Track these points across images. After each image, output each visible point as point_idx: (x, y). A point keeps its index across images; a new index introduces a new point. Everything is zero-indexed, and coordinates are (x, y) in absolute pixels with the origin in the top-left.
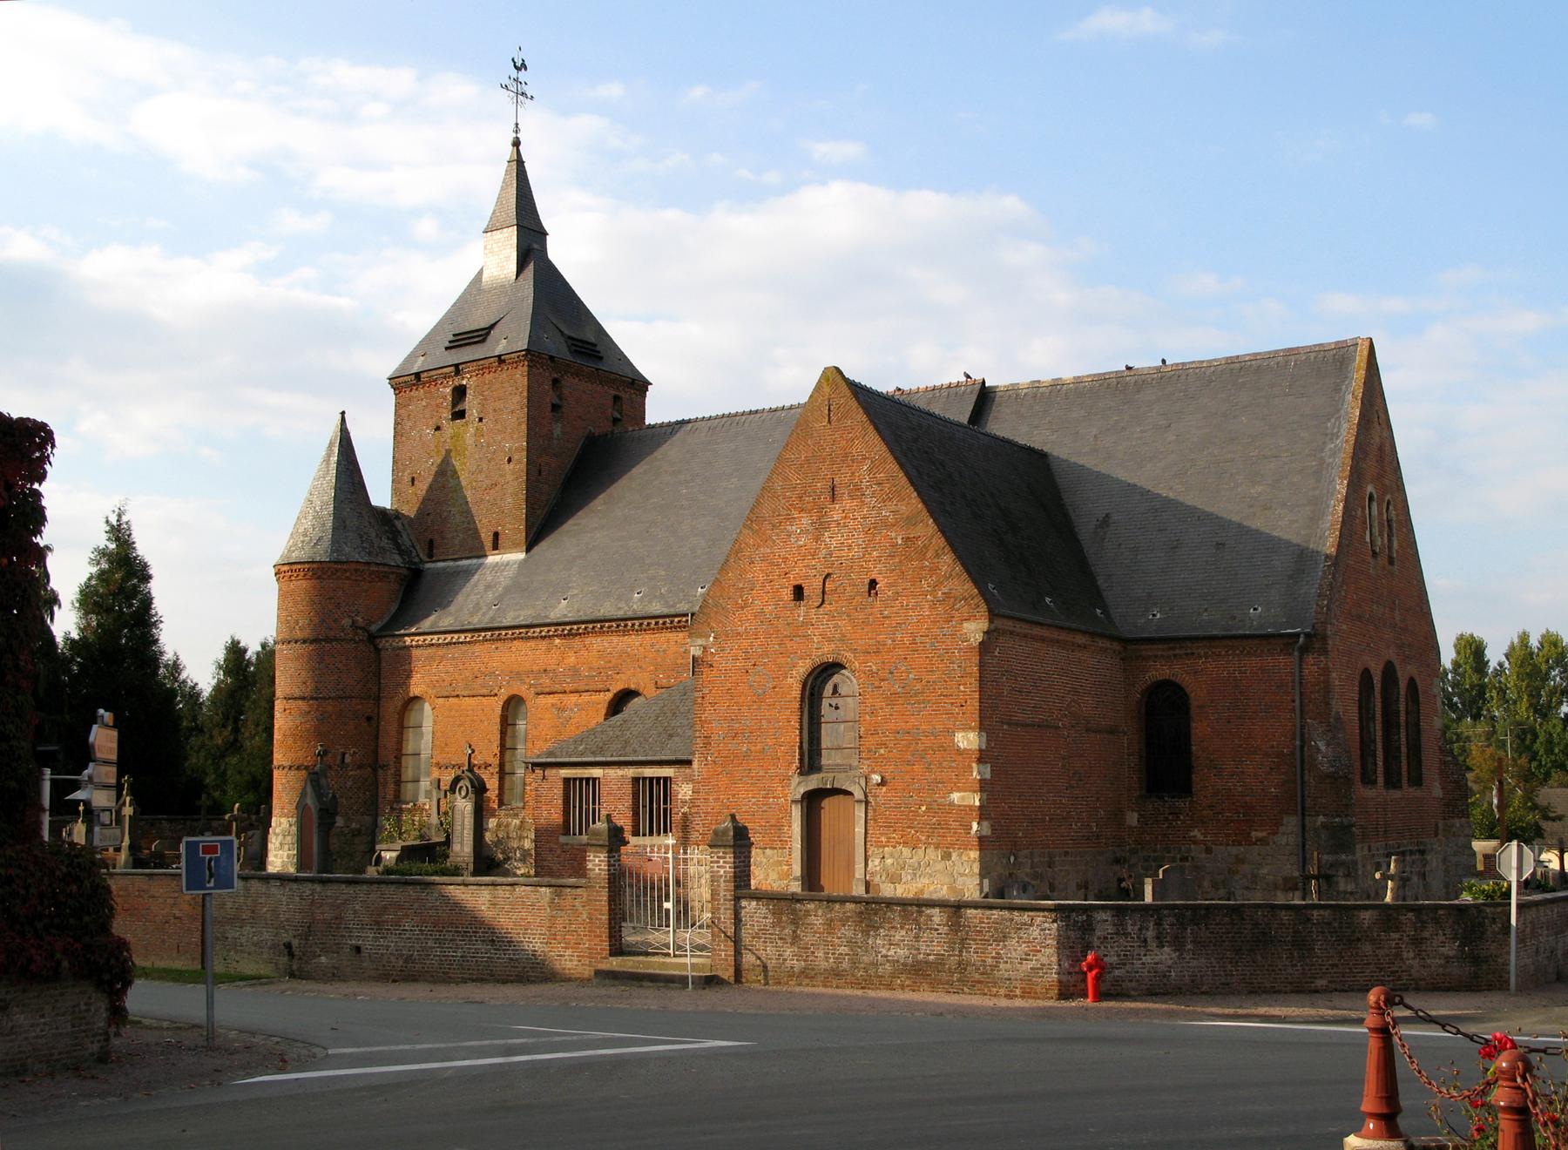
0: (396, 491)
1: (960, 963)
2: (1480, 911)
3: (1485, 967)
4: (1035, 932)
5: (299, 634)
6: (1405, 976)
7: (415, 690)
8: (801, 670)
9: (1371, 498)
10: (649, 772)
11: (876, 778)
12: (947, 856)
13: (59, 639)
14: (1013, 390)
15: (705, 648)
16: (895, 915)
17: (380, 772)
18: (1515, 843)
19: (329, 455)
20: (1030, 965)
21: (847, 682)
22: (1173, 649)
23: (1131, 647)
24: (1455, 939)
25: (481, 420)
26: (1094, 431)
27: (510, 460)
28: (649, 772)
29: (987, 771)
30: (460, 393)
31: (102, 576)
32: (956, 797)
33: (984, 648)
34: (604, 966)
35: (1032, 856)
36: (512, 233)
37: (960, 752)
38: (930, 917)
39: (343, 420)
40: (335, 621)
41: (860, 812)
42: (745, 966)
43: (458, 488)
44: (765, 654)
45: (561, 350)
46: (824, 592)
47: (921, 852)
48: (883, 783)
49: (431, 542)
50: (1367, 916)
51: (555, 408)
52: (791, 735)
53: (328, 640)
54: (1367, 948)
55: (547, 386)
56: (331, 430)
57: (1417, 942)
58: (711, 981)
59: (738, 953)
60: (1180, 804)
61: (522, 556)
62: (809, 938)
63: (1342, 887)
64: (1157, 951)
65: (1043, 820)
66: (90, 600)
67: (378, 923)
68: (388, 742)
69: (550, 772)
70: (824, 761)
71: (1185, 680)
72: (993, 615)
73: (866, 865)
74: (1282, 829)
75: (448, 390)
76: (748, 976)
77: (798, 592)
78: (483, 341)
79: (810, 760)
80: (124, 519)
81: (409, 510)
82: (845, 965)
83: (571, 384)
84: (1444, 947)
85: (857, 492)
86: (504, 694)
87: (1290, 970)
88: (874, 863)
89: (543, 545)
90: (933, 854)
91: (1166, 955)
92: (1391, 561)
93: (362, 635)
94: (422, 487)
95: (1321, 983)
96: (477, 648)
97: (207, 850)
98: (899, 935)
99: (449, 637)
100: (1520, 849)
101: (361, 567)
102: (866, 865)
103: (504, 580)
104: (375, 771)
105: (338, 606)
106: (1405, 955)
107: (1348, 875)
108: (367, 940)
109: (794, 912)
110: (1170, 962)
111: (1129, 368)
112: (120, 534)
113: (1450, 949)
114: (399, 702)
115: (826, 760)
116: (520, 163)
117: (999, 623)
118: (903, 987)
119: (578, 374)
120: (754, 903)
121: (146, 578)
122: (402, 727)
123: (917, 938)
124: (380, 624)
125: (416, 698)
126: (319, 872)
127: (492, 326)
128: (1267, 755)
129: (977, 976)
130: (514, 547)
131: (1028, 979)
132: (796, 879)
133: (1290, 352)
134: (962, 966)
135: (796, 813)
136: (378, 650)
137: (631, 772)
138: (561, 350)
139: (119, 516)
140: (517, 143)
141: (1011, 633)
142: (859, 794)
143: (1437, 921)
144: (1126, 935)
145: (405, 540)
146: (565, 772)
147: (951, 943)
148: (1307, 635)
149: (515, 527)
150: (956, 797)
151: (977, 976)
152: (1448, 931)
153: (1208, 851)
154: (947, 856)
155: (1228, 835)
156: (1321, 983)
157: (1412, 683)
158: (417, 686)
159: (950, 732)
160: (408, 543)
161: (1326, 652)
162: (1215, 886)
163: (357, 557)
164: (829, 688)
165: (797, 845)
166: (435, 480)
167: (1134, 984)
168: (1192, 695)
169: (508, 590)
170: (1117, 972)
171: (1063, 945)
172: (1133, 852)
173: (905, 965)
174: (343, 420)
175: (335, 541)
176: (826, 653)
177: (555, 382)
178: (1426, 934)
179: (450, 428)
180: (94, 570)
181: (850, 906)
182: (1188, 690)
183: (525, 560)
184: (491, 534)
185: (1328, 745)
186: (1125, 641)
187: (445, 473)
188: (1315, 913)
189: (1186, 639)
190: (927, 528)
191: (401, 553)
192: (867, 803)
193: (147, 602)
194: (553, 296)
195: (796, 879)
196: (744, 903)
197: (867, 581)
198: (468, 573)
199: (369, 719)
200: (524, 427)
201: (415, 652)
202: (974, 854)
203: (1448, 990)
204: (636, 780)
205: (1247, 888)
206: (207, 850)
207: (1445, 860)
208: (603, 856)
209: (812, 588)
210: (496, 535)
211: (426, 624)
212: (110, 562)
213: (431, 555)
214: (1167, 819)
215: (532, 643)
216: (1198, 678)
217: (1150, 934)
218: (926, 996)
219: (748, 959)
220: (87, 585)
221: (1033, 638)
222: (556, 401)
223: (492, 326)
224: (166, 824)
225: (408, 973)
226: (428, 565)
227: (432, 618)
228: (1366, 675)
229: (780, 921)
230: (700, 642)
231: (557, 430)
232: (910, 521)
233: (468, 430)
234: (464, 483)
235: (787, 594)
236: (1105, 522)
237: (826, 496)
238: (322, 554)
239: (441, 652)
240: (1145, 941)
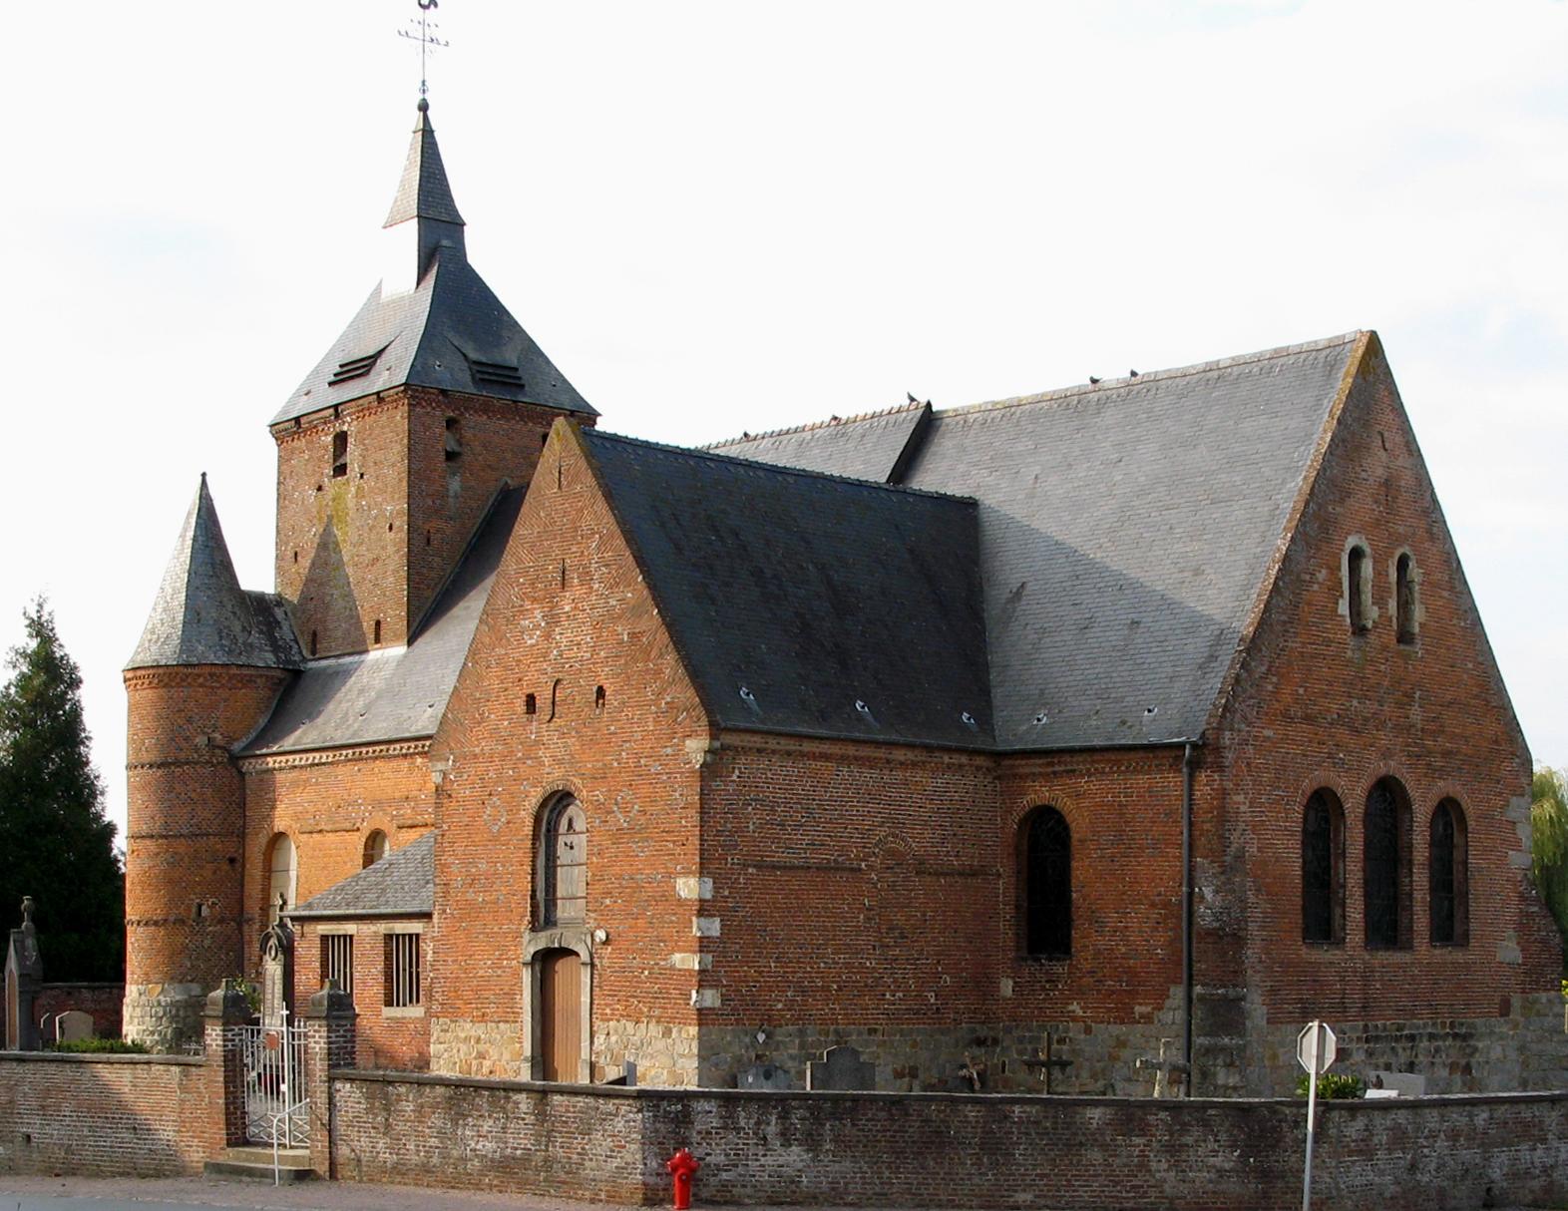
1: (545, 1161)
2: (1275, 1112)
3: (1280, 1184)
4: (620, 1124)
5: (146, 758)
6: (1153, 1193)
7: (280, 825)
8: (534, 801)
9: (1356, 555)
10: (400, 927)
11: (601, 935)
12: (667, 1033)
14: (962, 415)
16: (483, 1100)
17: (246, 928)
18: (1315, 1024)
19: (185, 530)
21: (577, 814)
22: (1052, 764)
23: (1005, 763)
24: (1233, 1147)
25: (362, 476)
27: (391, 528)
28: (400, 927)
29: (714, 927)
30: (341, 440)
32: (677, 959)
33: (710, 771)
34: (221, 1159)
35: (802, 1033)
38: (517, 1103)
39: (204, 483)
40: (186, 739)
42: (341, 1160)
43: (340, 564)
46: (553, 703)
47: (643, 1026)
48: (607, 942)
49: (315, 634)
50: (1096, 1115)
51: (450, 456)
52: (520, 884)
53: (177, 763)
54: (1095, 1156)
55: (439, 429)
57: (1173, 1150)
58: (302, 1176)
59: (332, 1143)
60: (1060, 969)
61: (400, 650)
62: (401, 1127)
64: (781, 1150)
65: (826, 989)
67: (43, 1107)
68: (253, 889)
70: (559, 913)
71: (1065, 804)
73: (592, 1043)
74: (1168, 1003)
75: (330, 438)
77: (531, 701)
78: (367, 373)
79: (543, 914)
81: (292, 595)
83: (475, 424)
86: (366, 829)
87: (976, 1180)
88: (600, 1039)
90: (655, 1030)
91: (794, 1157)
94: (305, 562)
98: (486, 1125)
99: (311, 756)
100: (1321, 1027)
101: (218, 671)
102: (592, 1043)
103: (378, 683)
104: (240, 925)
106: (1154, 1165)
107: (1229, 1065)
108: (34, 1126)
109: (386, 1096)
110: (800, 1165)
111: (1094, 381)
112: (41, 630)
113: (1226, 1160)
114: (264, 839)
116: (427, 134)
117: (729, 739)
118: (491, 1187)
119: (486, 409)
120: (348, 1086)
121: (75, 683)
122: (269, 870)
123: (504, 1128)
126: (21, 1050)
127: (380, 352)
128: (1153, 905)
129: (563, 1176)
130: (396, 638)
131: (612, 1181)
132: (526, 1059)
133: (1278, 354)
135: (526, 975)
136: (242, 775)
137: (382, 927)
139: (40, 606)
141: (759, 751)
142: (584, 956)
143: (1206, 1124)
144: (738, 1130)
145: (285, 633)
147: (538, 1135)
148: (1194, 746)
149: (396, 616)
151: (563, 1176)
152: (1223, 1137)
153: (1088, 1030)
154: (667, 1033)
155: (1110, 1010)
157: (1448, 812)
159: (670, 876)
160: (289, 637)
162: (1094, 1077)
163: (212, 659)
164: (564, 823)
166: (317, 555)
167: (749, 1191)
168: (1073, 826)
170: (724, 1176)
171: (651, 1141)
173: (492, 1160)
174: (204, 483)
175: (186, 639)
176: (554, 777)
177: (451, 424)
178: (1189, 1140)
179: (332, 486)
181: (440, 1090)
182: (1069, 819)
183: (405, 656)
184: (373, 623)
185: (1216, 892)
186: (999, 756)
187: (327, 545)
188: (1017, 1109)
189: (1061, 751)
190: (651, 619)
191: (276, 648)
192: (593, 965)
193: (76, 714)
195: (526, 1059)
196: (338, 1085)
197: (595, 689)
198: (345, 674)
199: (232, 861)
200: (405, 484)
201: (280, 777)
202: (693, 1030)
204: (388, 937)
205: (1129, 1080)
207: (1522, 1049)
208: (219, 1029)
210: (378, 623)
211: (288, 743)
212: (31, 663)
213: (314, 653)
214: (1043, 988)
215: (394, 764)
216: (1080, 801)
219: (343, 1151)
222: (452, 446)
223: (380, 352)
224: (86, 994)
225: (66, 1168)
226: (312, 665)
227: (298, 733)
229: (373, 1106)
230: (440, 766)
231: (455, 485)
232: (636, 612)
234: (345, 559)
235: (520, 706)
236: (1018, 595)
237: (556, 585)
238: (169, 654)
239: (306, 774)
240: (765, 1138)
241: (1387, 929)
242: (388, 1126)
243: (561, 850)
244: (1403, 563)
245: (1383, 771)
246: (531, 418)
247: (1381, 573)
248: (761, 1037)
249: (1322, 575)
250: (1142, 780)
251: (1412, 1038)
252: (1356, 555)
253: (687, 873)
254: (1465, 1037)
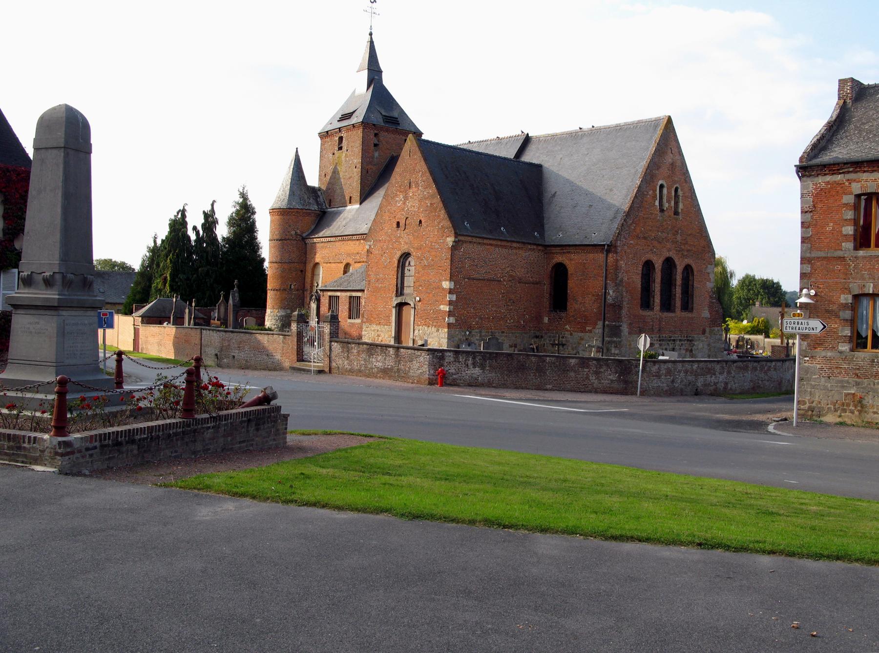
0: (320, 180)
4: (422, 359)
5: (275, 237)
6: (590, 387)
7: (317, 260)
9: (662, 186)
10: (354, 294)
11: (418, 299)
12: (438, 331)
13: (220, 239)
16: (379, 350)
23: (548, 249)
24: (616, 373)
26: (561, 156)
28: (354, 294)
29: (454, 298)
30: (341, 139)
33: (454, 248)
35: (480, 332)
36: (365, 73)
41: (412, 311)
43: (339, 178)
44: (387, 249)
45: (380, 121)
48: (420, 301)
51: (375, 145)
53: (285, 240)
54: (572, 374)
56: (292, 156)
57: (597, 373)
58: (320, 372)
60: (563, 314)
65: (489, 318)
66: (232, 222)
68: (308, 280)
69: (325, 293)
71: (566, 262)
72: (456, 235)
76: (334, 371)
77: (398, 224)
81: (324, 188)
83: (383, 135)
84: (610, 376)
86: (345, 262)
88: (416, 332)
90: (434, 329)
91: (477, 371)
93: (299, 238)
94: (328, 177)
95: (548, 387)
98: (379, 358)
107: (616, 347)
108: (236, 353)
114: (312, 265)
116: (372, 43)
117: (461, 238)
119: (387, 131)
121: (254, 213)
130: (356, 202)
131: (419, 376)
133: (639, 122)
135: (394, 311)
137: (349, 294)
138: (380, 121)
140: (371, 34)
142: (412, 305)
143: (608, 365)
145: (321, 199)
146: (330, 294)
148: (608, 245)
149: (356, 195)
150: (442, 307)
152: (613, 370)
153: (571, 334)
154: (438, 331)
156: (548, 387)
157: (688, 269)
161: (616, 253)
162: (573, 349)
165: (393, 324)
169: (350, 220)
175: (289, 200)
176: (405, 248)
177: (376, 135)
179: (337, 153)
187: (335, 172)
191: (318, 204)
193: (254, 223)
198: (339, 213)
201: (318, 245)
202: (446, 330)
203: (612, 393)
204: (350, 297)
206: (104, 315)
207: (709, 345)
209: (402, 224)
211: (321, 234)
216: (571, 262)
217: (470, 362)
218: (387, 382)
219: (334, 364)
220: (232, 216)
222: (376, 142)
224: (254, 312)
231: (376, 154)
232: (432, 197)
233: (343, 154)
235: (395, 225)
236: (554, 195)
237: (407, 187)
238: (284, 205)
239: (326, 244)
250: (591, 256)
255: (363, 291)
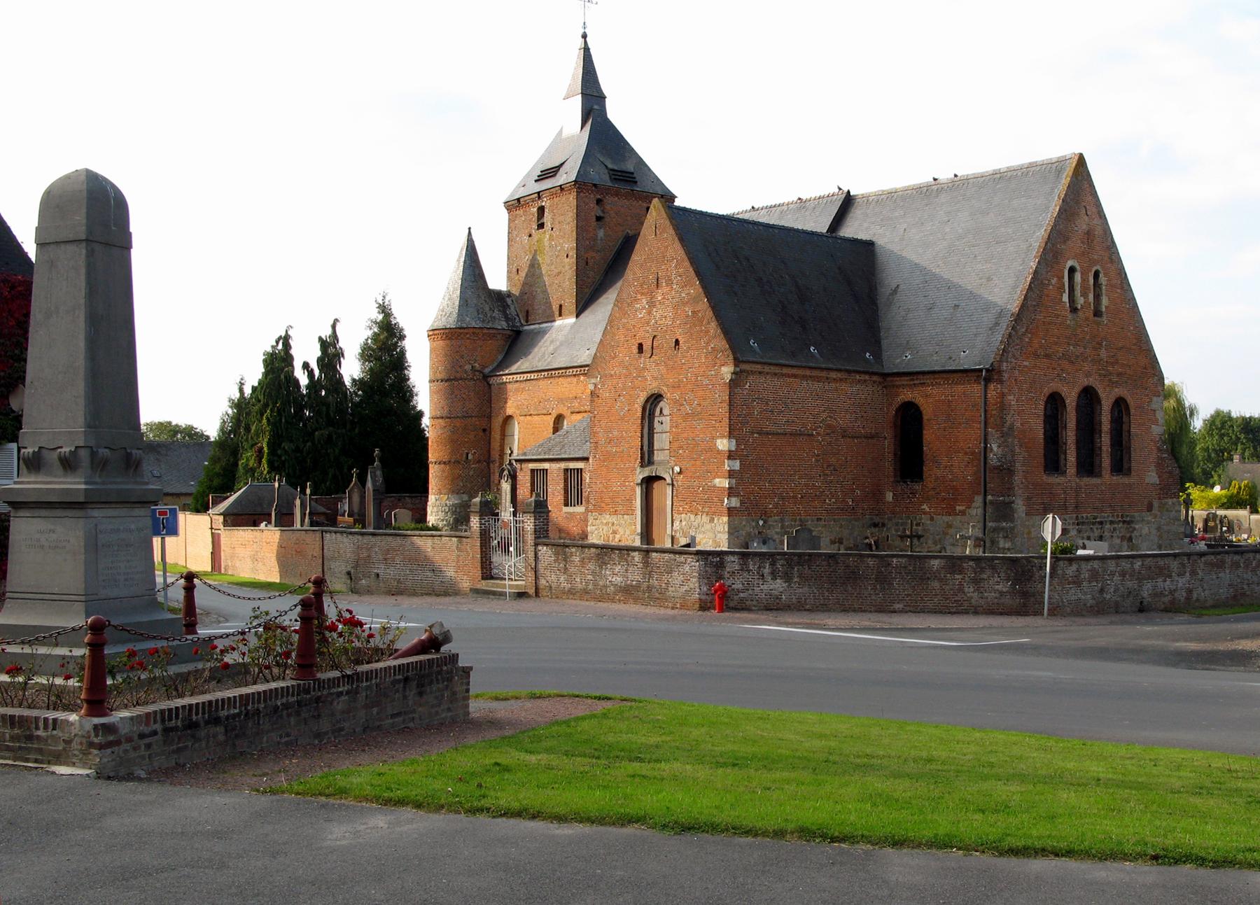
4: (687, 568)
6: (966, 604)
7: (509, 411)
9: (1072, 270)
10: (572, 465)
11: (677, 469)
12: (712, 520)
15: (596, 385)
20: (686, 588)
23: (888, 379)
24: (1008, 580)
28: (572, 465)
29: (736, 465)
30: (541, 210)
31: (375, 337)
32: (717, 481)
33: (734, 384)
34: (479, 586)
35: (782, 520)
37: (719, 452)
41: (669, 490)
45: (603, 178)
48: (680, 473)
50: (936, 563)
51: (599, 219)
52: (633, 442)
53: (456, 379)
54: (936, 584)
55: (593, 204)
57: (976, 581)
58: (521, 595)
59: (536, 578)
60: (917, 487)
61: (572, 320)
63: (1001, 546)
65: (795, 497)
66: (367, 354)
68: (495, 445)
70: (655, 458)
71: (920, 401)
77: (640, 346)
79: (647, 458)
80: (387, 299)
82: (590, 587)
83: (610, 201)
84: (998, 586)
85: (669, 282)
88: (677, 524)
89: (583, 315)
90: (705, 519)
92: (1097, 313)
94: (523, 274)
95: (898, 606)
96: (541, 383)
97: (161, 513)
98: (618, 568)
104: (488, 464)
105: (462, 357)
107: (1005, 537)
109: (565, 553)
112: (385, 310)
113: (1004, 587)
114: (500, 419)
115: (658, 457)
124: (491, 368)
125: (510, 417)
128: (966, 453)
130: (570, 314)
133: (1031, 165)
134: (649, 588)
135: (638, 490)
136: (490, 385)
137: (563, 465)
138: (603, 178)
140: (584, 36)
142: (669, 480)
143: (993, 568)
144: (749, 571)
145: (512, 311)
148: (987, 370)
149: (570, 303)
152: (1002, 575)
153: (932, 519)
154: (712, 520)
156: (898, 606)
157: (1120, 405)
158: (510, 410)
163: (474, 324)
169: (561, 344)
172: (890, 519)
175: (460, 314)
177: (599, 202)
178: (985, 576)
179: (537, 234)
180: (370, 333)
181: (593, 550)
186: (885, 376)
188: (895, 560)
191: (507, 319)
193: (402, 354)
194: (604, 138)
198: (543, 333)
199: (484, 430)
201: (509, 386)
202: (725, 519)
203: (1001, 614)
204: (566, 470)
206: (161, 513)
207: (1159, 529)
211: (514, 369)
212: (380, 327)
215: (569, 379)
216: (928, 399)
217: (767, 571)
218: (632, 608)
219: (542, 582)
220: (366, 344)
221: (783, 375)
222: (600, 214)
228: (1055, 401)
230: (593, 381)
231: (601, 233)
232: (695, 300)
233: (546, 234)
235: (635, 350)
236: (895, 291)
237: (653, 286)
238: (451, 322)
239: (523, 385)
241: (1088, 466)
242: (566, 569)
243: (656, 425)
244: (1096, 275)
245: (1086, 383)
246: (640, 199)
247: (1084, 280)
248: (761, 523)
249: (1054, 281)
250: (960, 388)
251: (1101, 523)
252: (1072, 270)
253: (722, 437)
254: (1129, 523)
255: (587, 459)
